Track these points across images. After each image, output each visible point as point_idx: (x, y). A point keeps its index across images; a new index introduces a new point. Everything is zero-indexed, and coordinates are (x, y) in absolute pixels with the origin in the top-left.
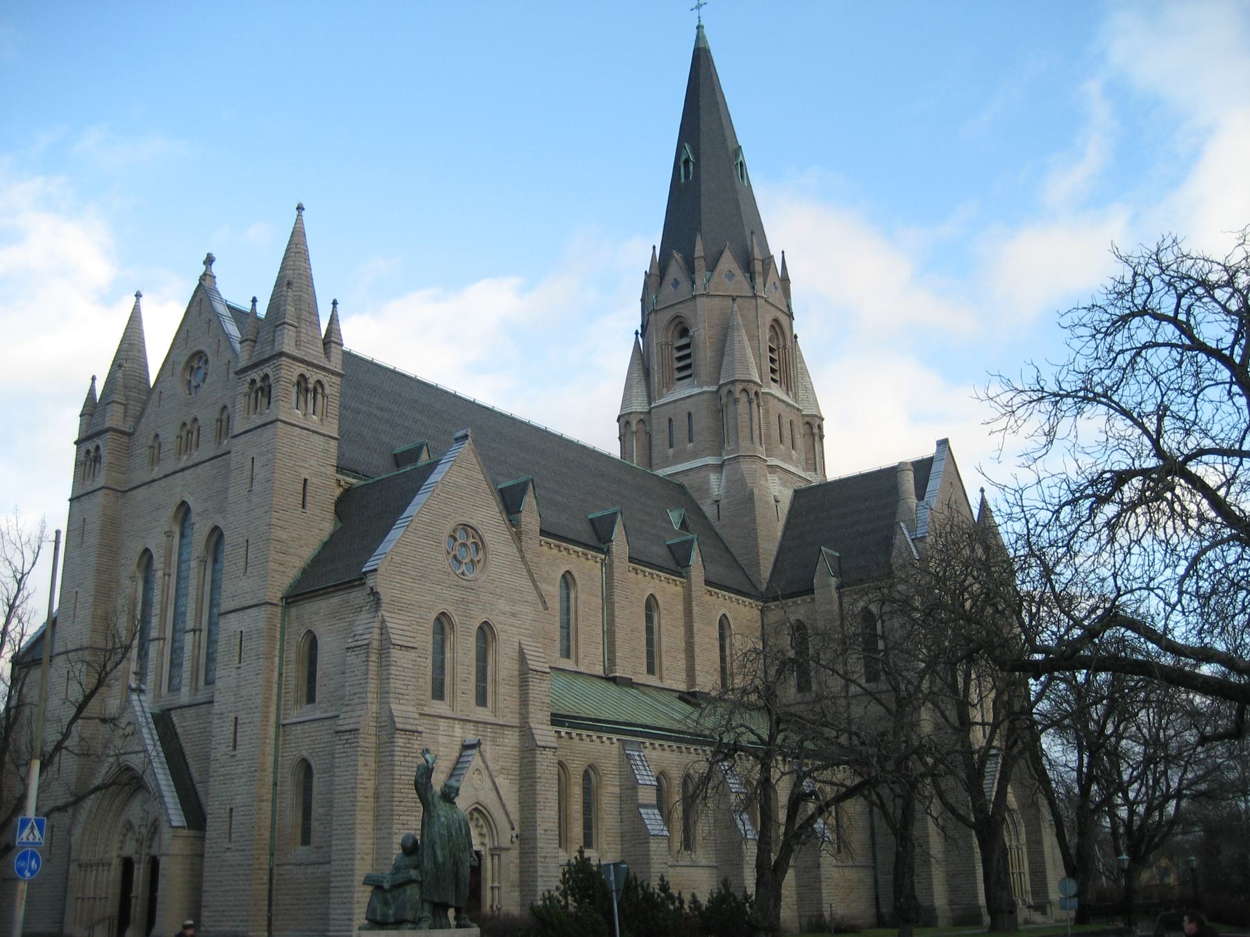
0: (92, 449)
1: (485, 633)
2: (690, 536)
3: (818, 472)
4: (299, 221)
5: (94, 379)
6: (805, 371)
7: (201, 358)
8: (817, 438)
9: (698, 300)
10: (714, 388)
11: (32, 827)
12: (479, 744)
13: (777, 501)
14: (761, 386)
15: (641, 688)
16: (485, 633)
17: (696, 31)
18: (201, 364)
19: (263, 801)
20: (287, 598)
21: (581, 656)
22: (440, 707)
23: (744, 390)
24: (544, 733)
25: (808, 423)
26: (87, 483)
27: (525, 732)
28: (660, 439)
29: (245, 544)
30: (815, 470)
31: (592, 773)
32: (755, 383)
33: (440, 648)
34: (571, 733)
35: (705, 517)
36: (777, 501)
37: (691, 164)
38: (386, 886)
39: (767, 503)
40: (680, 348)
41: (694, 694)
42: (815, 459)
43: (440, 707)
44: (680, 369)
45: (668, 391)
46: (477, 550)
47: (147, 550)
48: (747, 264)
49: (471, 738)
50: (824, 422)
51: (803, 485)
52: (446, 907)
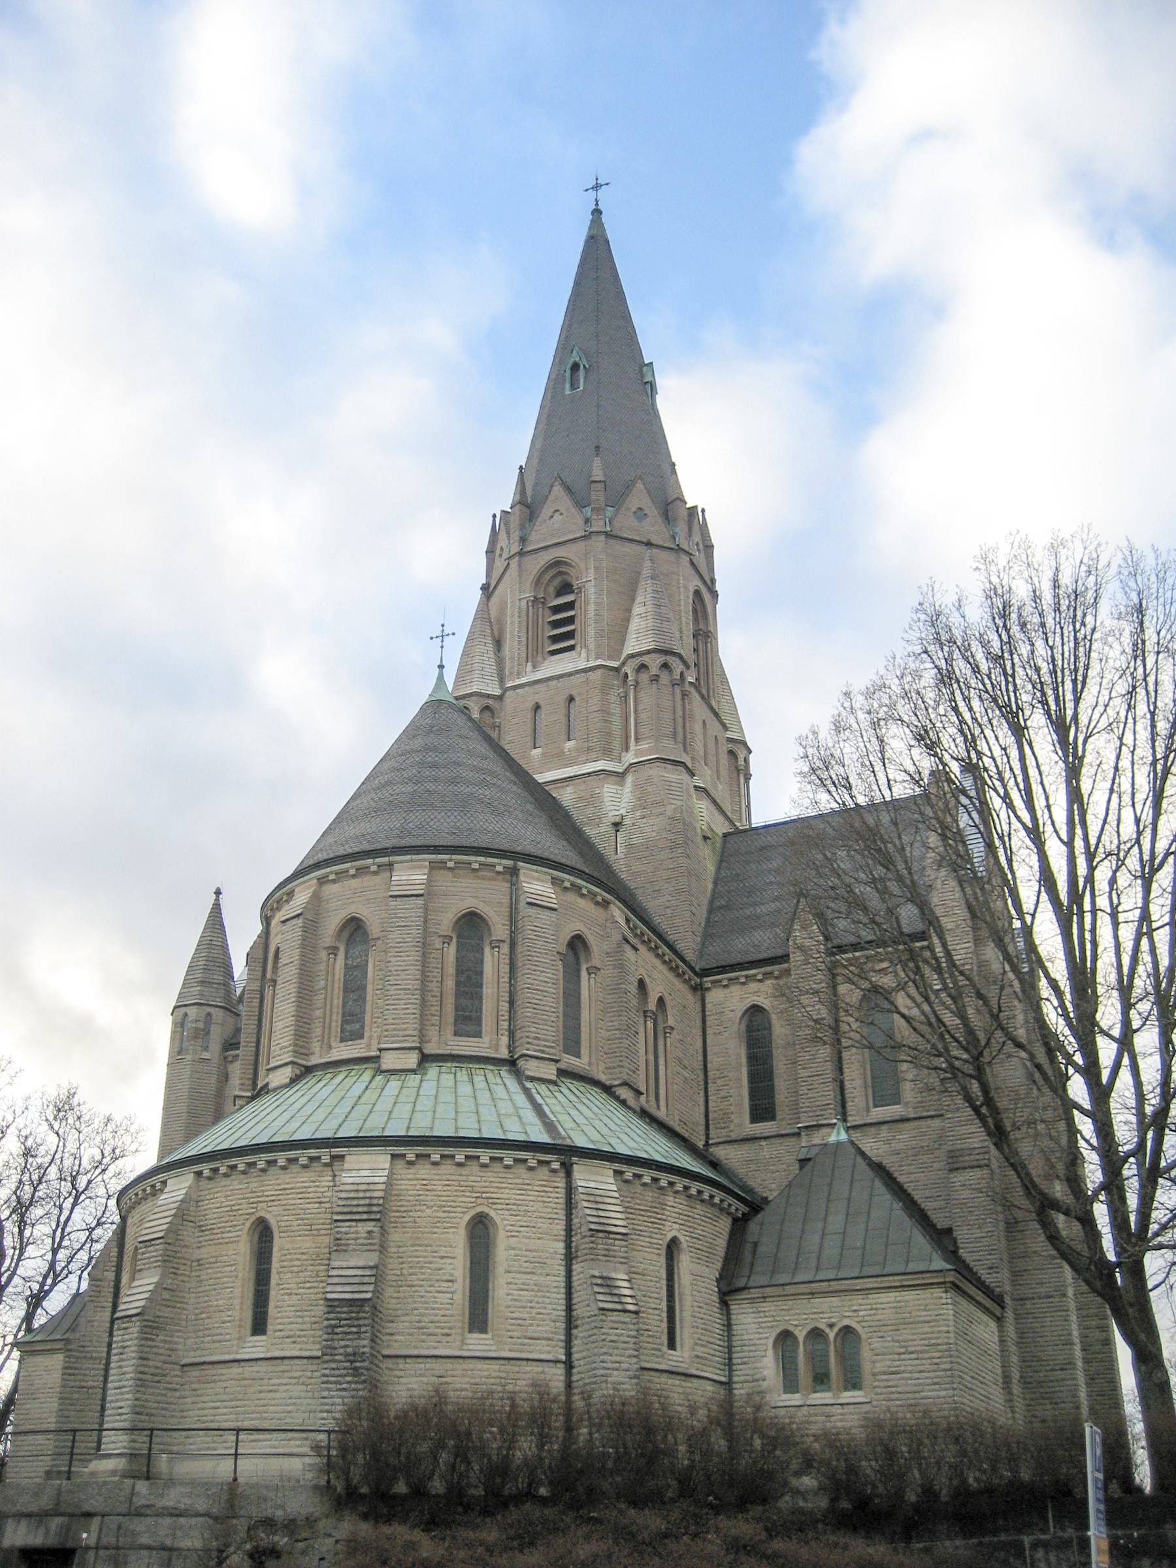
6: (725, 681)
9: (594, 538)
22: (275, 1464)
40: (556, 609)
43: (275, 1464)
44: (555, 639)
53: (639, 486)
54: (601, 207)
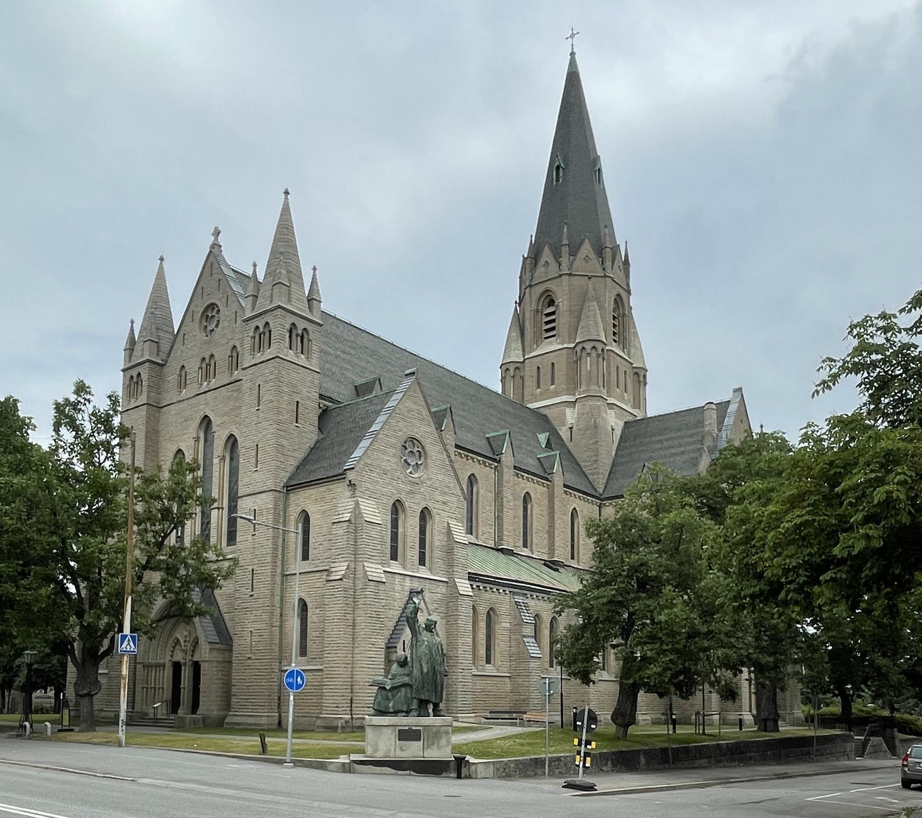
0: (135, 376)
1: (425, 515)
2: (553, 453)
3: (642, 408)
4: (161, 268)
5: (132, 322)
7: (214, 308)
8: (642, 384)
9: (563, 277)
10: (572, 345)
11: (129, 640)
12: (422, 591)
13: (613, 430)
14: (605, 344)
15: (519, 556)
16: (425, 515)
17: (569, 57)
18: (214, 314)
19: (273, 626)
20: (287, 487)
21: (480, 533)
23: (594, 347)
24: (464, 587)
25: (636, 373)
26: (133, 400)
27: (451, 584)
28: (530, 383)
29: (255, 448)
30: (640, 408)
31: (491, 613)
32: (603, 342)
33: (395, 524)
34: (479, 586)
35: (562, 440)
36: (613, 430)
37: (561, 169)
38: (388, 688)
39: (606, 429)
40: (548, 315)
41: (553, 562)
42: (639, 401)
44: (547, 331)
45: (537, 346)
46: (420, 456)
47: (180, 450)
48: (600, 251)
49: (417, 585)
50: (648, 373)
51: (631, 418)
52: (427, 702)
53: (587, 240)
54: (575, 50)
